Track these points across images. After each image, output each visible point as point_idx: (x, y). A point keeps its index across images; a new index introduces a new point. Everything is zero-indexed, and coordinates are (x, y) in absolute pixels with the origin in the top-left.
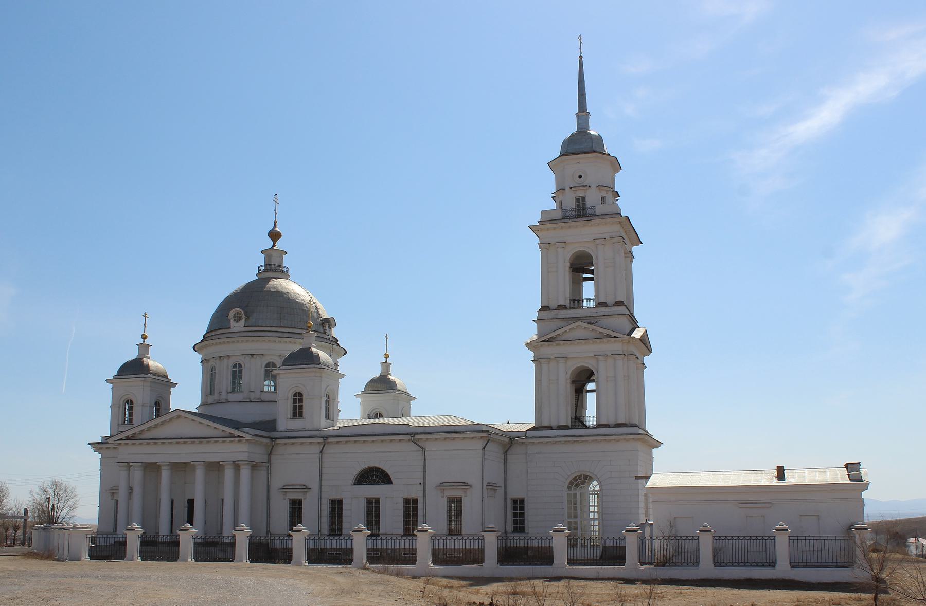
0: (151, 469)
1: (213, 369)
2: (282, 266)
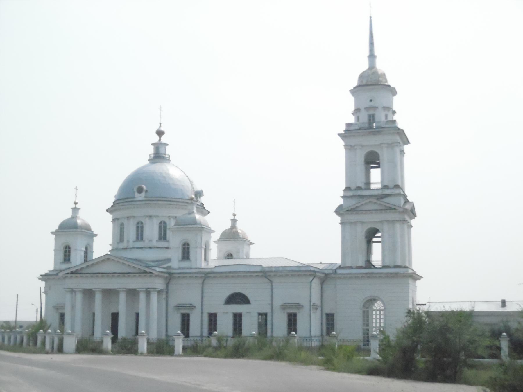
0: (89, 294)
1: (122, 225)
2: (165, 154)
